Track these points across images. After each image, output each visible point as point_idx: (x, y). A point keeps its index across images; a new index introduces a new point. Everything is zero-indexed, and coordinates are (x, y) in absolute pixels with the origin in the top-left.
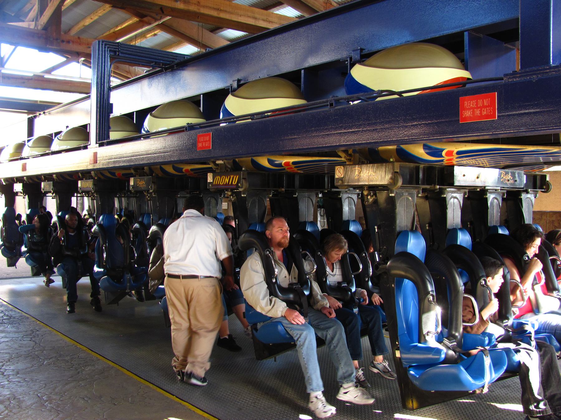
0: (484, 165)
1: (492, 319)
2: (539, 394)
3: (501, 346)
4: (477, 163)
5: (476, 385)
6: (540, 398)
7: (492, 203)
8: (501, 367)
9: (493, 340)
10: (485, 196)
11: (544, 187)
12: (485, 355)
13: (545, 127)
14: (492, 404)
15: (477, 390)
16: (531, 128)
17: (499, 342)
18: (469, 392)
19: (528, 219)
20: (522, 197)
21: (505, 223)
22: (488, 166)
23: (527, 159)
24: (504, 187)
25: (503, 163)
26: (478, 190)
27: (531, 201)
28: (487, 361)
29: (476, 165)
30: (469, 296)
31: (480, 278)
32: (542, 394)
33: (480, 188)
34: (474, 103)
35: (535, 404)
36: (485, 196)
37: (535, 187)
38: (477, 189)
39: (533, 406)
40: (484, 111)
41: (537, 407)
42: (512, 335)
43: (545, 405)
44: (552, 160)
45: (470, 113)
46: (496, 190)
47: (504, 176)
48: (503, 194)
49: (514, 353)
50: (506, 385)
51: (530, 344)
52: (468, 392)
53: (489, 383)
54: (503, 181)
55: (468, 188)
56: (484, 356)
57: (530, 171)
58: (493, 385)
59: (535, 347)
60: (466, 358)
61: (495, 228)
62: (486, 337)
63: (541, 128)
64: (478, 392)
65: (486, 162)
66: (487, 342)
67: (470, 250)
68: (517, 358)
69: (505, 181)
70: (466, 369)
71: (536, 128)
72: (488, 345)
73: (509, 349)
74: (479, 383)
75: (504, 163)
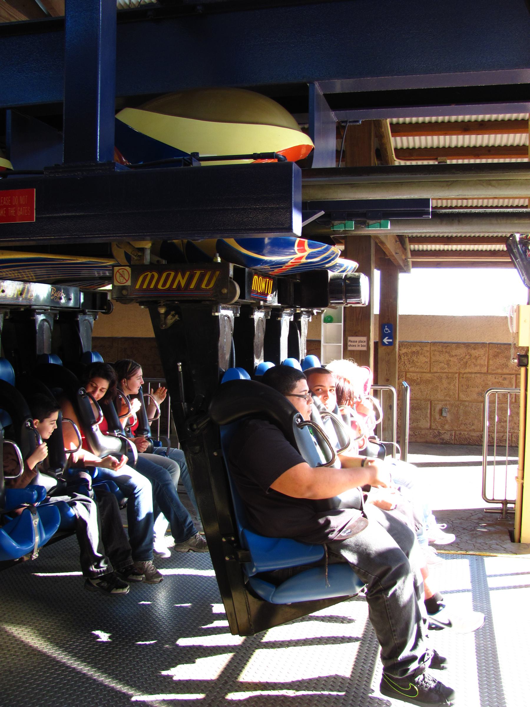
0: (30, 279)
1: (42, 468)
2: (98, 552)
3: (54, 499)
4: (20, 276)
5: (22, 550)
6: (100, 555)
7: (41, 326)
8: (54, 525)
9: (43, 494)
10: (32, 318)
11: (105, 307)
12: (32, 513)
13: (90, 235)
14: (35, 574)
15: (25, 557)
16: (75, 235)
17: (52, 495)
18: (15, 560)
19: (86, 344)
20: (78, 319)
21: (56, 351)
22: (35, 280)
23: (85, 273)
24: (56, 307)
25: (53, 277)
26: (22, 309)
27: (90, 323)
28: (36, 521)
29: (19, 278)
30: (11, 443)
31: (24, 419)
32: (103, 551)
33: (24, 307)
34: (8, 200)
35: (96, 564)
36: (32, 318)
37: (94, 307)
38: (20, 308)
39: (93, 567)
40: (19, 210)
41: (98, 567)
42: (68, 485)
43: (106, 563)
44: (108, 275)
45: (3, 212)
46: (45, 310)
47: (54, 293)
48: (55, 316)
49: (68, 506)
50: (68, 548)
51: (88, 495)
52: (13, 560)
53: (39, 546)
54: (53, 299)
55: (10, 307)
56: (31, 515)
57: (88, 287)
58: (45, 546)
59: (94, 497)
60: (11, 519)
61: (45, 357)
62: (34, 491)
63: (85, 235)
64: (26, 559)
65: (32, 275)
66: (35, 497)
67: (14, 385)
68: (73, 511)
69: (56, 299)
70: (10, 534)
71: (80, 235)
72: (37, 501)
73: (62, 502)
74: (26, 548)
75: (55, 277)
